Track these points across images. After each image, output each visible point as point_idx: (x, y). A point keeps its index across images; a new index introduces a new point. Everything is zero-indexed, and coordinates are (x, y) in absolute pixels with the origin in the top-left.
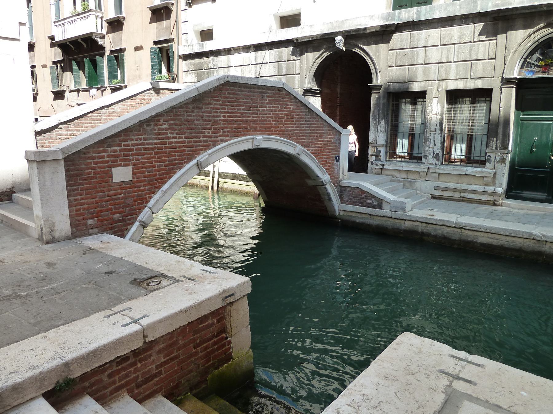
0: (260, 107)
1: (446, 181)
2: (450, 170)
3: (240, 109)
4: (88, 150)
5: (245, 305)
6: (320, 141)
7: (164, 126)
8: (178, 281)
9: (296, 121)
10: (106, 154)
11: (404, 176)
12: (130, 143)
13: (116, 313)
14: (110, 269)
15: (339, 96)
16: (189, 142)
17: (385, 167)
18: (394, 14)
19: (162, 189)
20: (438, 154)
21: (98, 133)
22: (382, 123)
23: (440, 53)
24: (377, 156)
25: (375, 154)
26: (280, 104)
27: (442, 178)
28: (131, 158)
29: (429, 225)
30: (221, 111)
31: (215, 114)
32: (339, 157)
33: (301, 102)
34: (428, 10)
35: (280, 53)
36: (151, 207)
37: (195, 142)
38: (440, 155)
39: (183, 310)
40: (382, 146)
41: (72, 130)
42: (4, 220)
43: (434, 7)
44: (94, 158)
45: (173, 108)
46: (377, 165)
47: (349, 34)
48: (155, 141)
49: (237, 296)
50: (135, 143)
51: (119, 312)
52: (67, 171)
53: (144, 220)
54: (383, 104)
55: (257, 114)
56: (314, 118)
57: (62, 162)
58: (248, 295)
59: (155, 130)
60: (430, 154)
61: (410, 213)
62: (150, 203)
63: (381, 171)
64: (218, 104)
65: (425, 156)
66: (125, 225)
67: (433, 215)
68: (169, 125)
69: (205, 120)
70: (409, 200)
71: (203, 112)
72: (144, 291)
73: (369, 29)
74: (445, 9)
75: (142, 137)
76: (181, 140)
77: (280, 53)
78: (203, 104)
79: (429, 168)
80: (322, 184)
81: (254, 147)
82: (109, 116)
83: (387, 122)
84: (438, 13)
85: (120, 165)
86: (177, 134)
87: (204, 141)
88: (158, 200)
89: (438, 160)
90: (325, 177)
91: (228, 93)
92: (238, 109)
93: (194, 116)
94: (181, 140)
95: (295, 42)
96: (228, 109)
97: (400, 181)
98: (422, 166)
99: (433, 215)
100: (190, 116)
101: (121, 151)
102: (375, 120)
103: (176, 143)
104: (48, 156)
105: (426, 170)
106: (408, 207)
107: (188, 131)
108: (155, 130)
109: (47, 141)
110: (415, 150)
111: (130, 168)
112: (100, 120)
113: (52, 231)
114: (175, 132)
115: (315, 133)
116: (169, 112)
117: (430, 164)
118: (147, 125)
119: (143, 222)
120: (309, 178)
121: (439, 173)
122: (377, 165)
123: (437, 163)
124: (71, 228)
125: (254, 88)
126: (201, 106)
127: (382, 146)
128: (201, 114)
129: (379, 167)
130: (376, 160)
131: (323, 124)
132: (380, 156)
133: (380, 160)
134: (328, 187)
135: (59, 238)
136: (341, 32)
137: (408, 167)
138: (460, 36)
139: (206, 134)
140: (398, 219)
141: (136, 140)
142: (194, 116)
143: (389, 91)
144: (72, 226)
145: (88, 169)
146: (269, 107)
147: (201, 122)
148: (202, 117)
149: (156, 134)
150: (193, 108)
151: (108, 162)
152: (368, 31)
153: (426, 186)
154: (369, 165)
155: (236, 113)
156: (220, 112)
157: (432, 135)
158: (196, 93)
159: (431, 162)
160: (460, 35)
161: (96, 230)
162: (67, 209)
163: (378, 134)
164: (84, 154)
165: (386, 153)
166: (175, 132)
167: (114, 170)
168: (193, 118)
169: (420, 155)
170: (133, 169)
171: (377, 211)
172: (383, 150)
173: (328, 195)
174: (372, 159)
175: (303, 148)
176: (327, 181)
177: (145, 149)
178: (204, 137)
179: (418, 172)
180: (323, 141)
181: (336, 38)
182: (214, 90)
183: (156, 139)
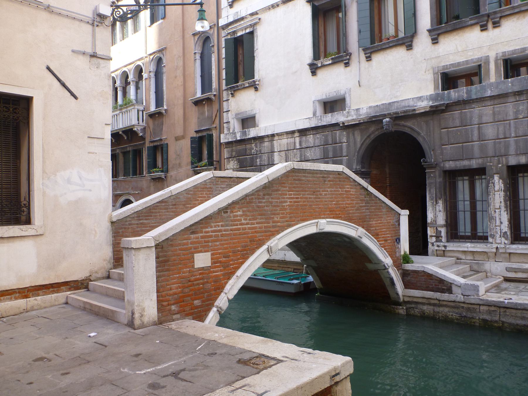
0: (323, 191)
1: (519, 261)
2: (522, 249)
3: (305, 194)
4: (175, 238)
5: (348, 385)
6: (379, 223)
7: (239, 213)
8: (282, 361)
9: (357, 203)
10: (189, 241)
11: (470, 257)
12: (210, 230)
13: (237, 389)
14: (211, 351)
15: (388, 176)
16: (260, 228)
17: (448, 249)
18: (444, 94)
19: (236, 274)
20: (506, 232)
21: (184, 221)
22: (441, 203)
23: (496, 129)
24: (438, 237)
25: (435, 234)
26: (340, 188)
27: (513, 258)
28: (210, 244)
29: (508, 310)
30: (288, 196)
31: (283, 200)
32: (399, 240)
33: (360, 185)
34: (479, 88)
35: (326, 136)
36: (227, 292)
37: (265, 227)
38: (508, 234)
39: (300, 386)
40: (442, 226)
41: (142, 219)
42: (87, 306)
43: (485, 86)
44: (180, 245)
45: (247, 196)
46: (438, 246)
47: (398, 115)
48: (231, 227)
49: (342, 376)
50: (214, 230)
51: (240, 388)
52: (157, 258)
53: (221, 305)
54: (440, 182)
55: (319, 198)
56: (373, 200)
57: (154, 249)
58: (350, 375)
59: (231, 217)
60: (497, 232)
61: (484, 297)
62: (225, 288)
63: (443, 254)
64: (285, 190)
65: (491, 235)
66: (203, 311)
67: (511, 299)
68: (243, 211)
69: (275, 206)
70: (481, 282)
71: (272, 198)
72: (255, 371)
73: (418, 110)
74: (497, 87)
75: (220, 224)
76: (253, 226)
77: (326, 136)
78: (272, 191)
79: (497, 248)
80: (384, 268)
81: (318, 231)
82: (175, 205)
83: (445, 202)
84: (489, 92)
85: (201, 252)
86: (250, 220)
87: (273, 227)
88: (233, 286)
89: (506, 239)
90: (387, 261)
91: (294, 179)
92: (303, 195)
93: (264, 203)
94: (253, 226)
95: (341, 125)
96: (294, 194)
97: (466, 264)
98: (489, 245)
99: (511, 299)
100: (260, 202)
101: (202, 237)
102: (432, 199)
103: (249, 228)
104: (143, 244)
105: (495, 250)
106: (482, 291)
107: (259, 217)
108: (231, 217)
109: (121, 231)
110: (480, 229)
111: (209, 254)
112: (167, 209)
113: (142, 316)
114: (248, 218)
115: (375, 215)
116: (243, 199)
117: (499, 244)
118: (224, 212)
119: (220, 308)
120: (370, 261)
121: (510, 254)
122: (438, 246)
123: (506, 242)
124: (158, 313)
125: (317, 174)
126: (270, 192)
127: (442, 226)
128: (270, 200)
129: (440, 248)
130: (436, 241)
131: (381, 206)
132: (442, 237)
133: (441, 241)
134: (390, 270)
135: (147, 323)
136: (389, 114)
137: (474, 247)
138: (516, 112)
139: (276, 219)
140: (471, 304)
141: (215, 227)
142: (264, 203)
143: (445, 169)
144: (159, 310)
145: (174, 255)
146: (331, 191)
147: (270, 208)
148: (271, 203)
149: (232, 221)
150: (264, 195)
151: (191, 248)
152: (417, 112)
153: (498, 268)
154: (430, 246)
155: (301, 198)
156: (287, 198)
157: (497, 213)
158: (266, 181)
159: (499, 242)
160: (515, 110)
161: (178, 316)
162: (156, 294)
163: (436, 214)
164: (171, 241)
165: (447, 233)
166: (248, 218)
167: (196, 255)
168: (263, 204)
169: (485, 234)
170: (212, 255)
171: (446, 296)
172: (443, 231)
173: (392, 280)
174: (432, 240)
175: (364, 231)
176: (389, 265)
177: (222, 235)
178: (273, 222)
179: (485, 252)
180: (382, 223)
181: (384, 120)
182: (282, 177)
183: (232, 225)
